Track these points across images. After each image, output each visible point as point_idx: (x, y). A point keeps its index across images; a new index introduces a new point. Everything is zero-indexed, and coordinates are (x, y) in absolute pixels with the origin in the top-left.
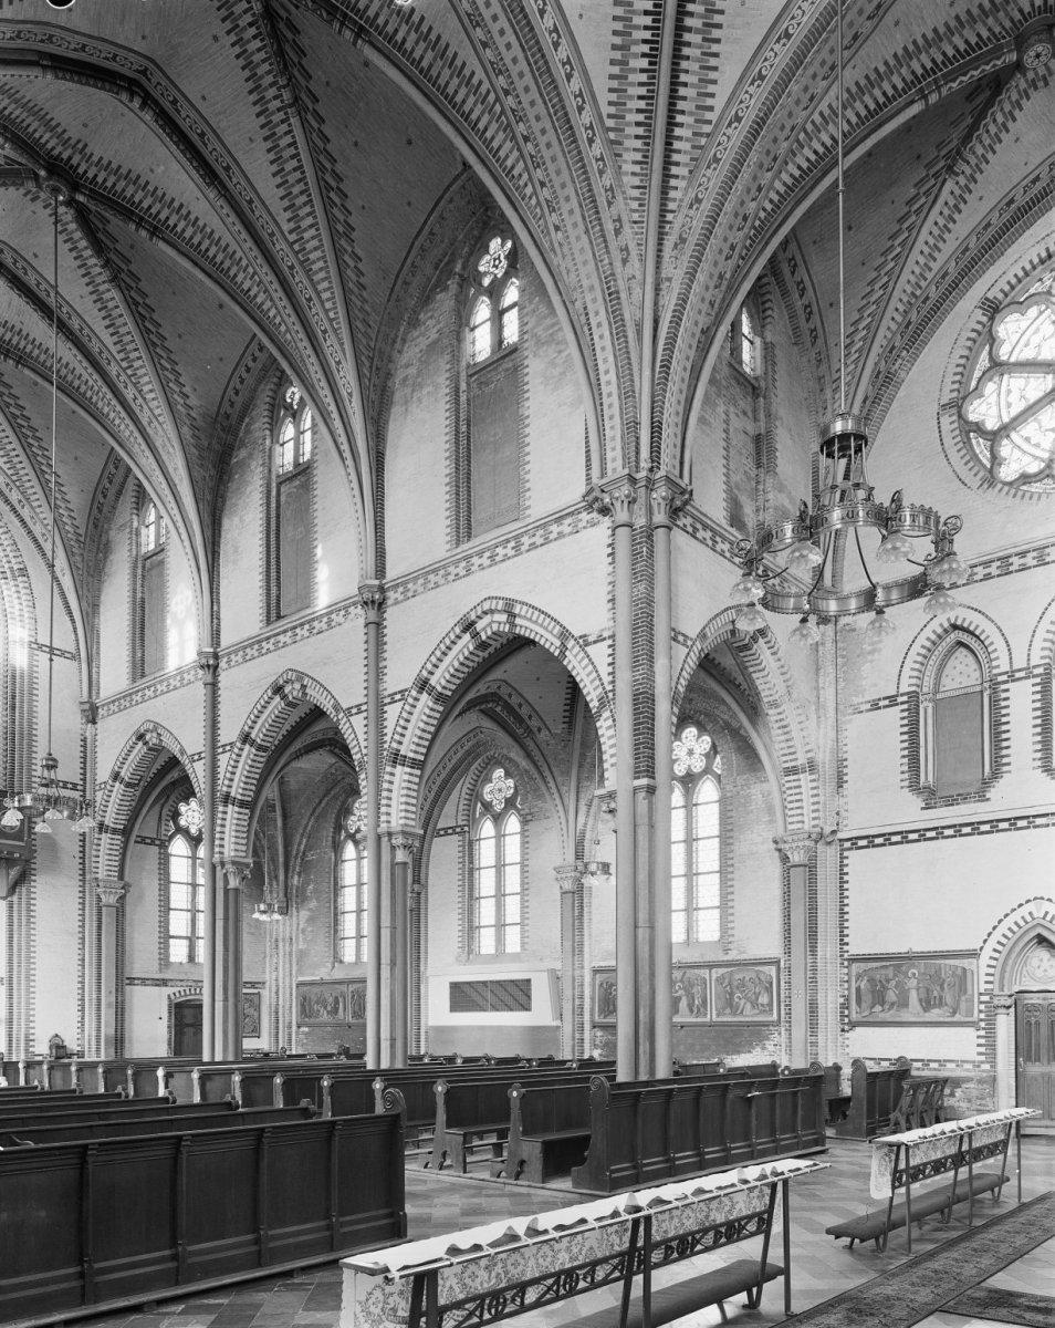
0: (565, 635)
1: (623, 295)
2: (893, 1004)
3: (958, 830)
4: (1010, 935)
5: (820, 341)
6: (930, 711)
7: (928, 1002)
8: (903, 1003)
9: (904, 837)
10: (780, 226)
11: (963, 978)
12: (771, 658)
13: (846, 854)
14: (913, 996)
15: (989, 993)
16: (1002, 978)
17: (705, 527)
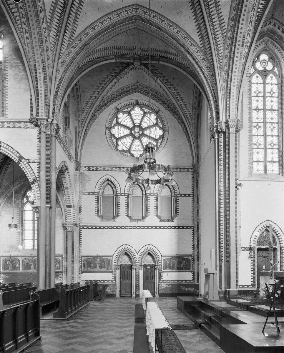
0: (21, 158)
1: (47, 68)
2: (93, 267)
3: (109, 227)
4: (121, 251)
5: (79, 99)
6: (102, 198)
7: (101, 267)
8: (95, 267)
9: (96, 227)
10: (84, 71)
11: (109, 261)
12: (68, 176)
13: (81, 229)
14: (98, 265)
15: (115, 265)
16: (118, 262)
17: (60, 139)
